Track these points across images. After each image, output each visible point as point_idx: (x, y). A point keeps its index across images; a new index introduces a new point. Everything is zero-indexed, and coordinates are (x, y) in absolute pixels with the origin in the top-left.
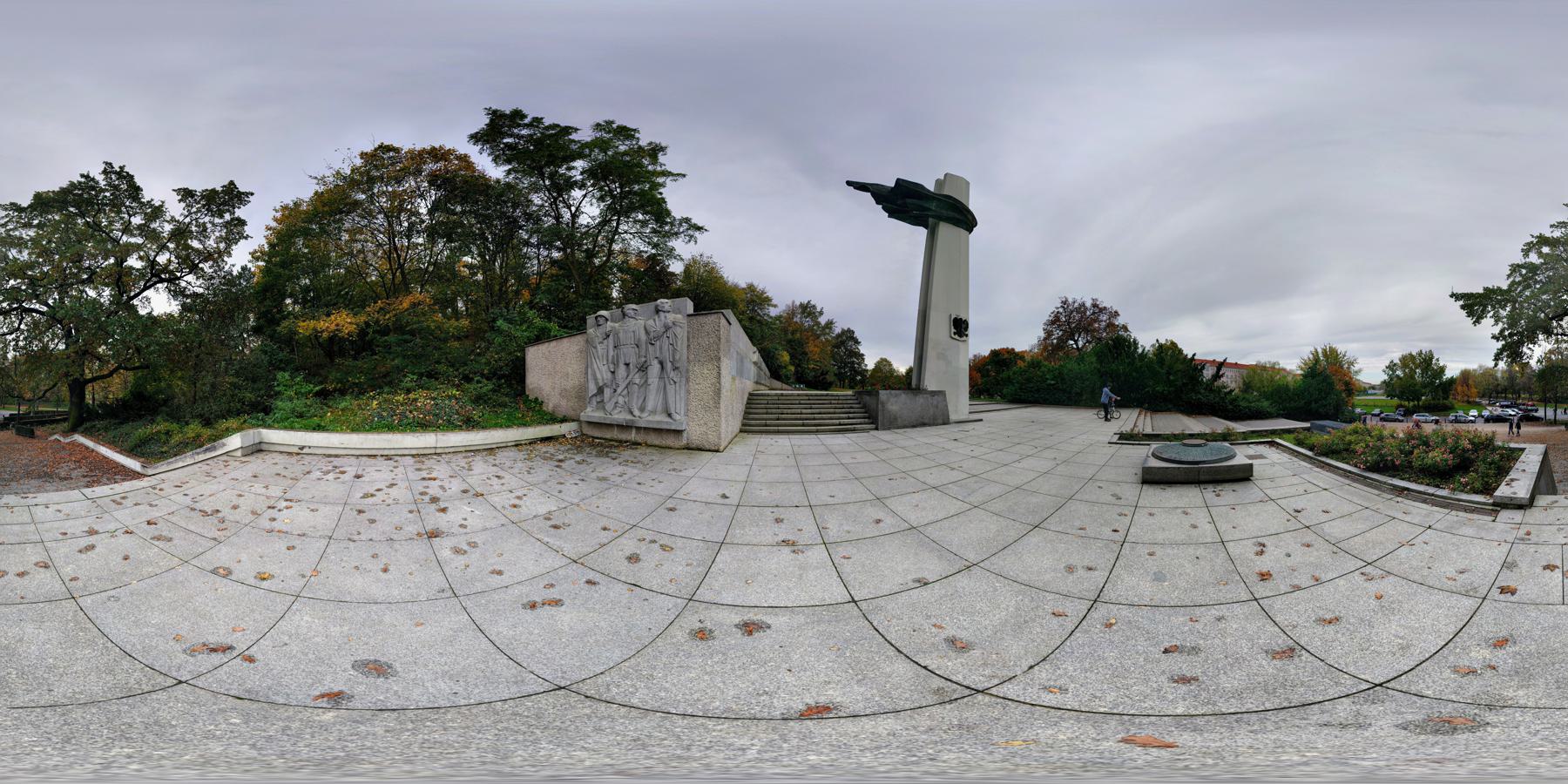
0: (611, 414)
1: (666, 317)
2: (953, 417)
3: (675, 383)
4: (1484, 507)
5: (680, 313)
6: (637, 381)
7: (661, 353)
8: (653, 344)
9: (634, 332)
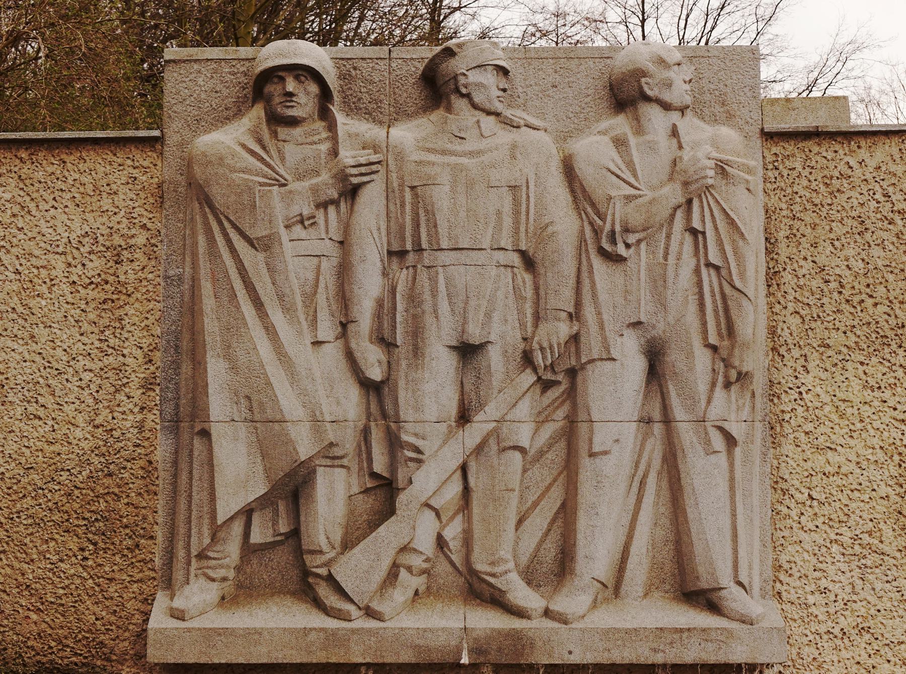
0: (370, 613)
1: (674, 132)
2: (387, 618)
3: (730, 441)
4: (238, 285)
5: (729, 118)
6: (524, 435)
7: (662, 303)
8: (618, 259)
9: (513, 188)
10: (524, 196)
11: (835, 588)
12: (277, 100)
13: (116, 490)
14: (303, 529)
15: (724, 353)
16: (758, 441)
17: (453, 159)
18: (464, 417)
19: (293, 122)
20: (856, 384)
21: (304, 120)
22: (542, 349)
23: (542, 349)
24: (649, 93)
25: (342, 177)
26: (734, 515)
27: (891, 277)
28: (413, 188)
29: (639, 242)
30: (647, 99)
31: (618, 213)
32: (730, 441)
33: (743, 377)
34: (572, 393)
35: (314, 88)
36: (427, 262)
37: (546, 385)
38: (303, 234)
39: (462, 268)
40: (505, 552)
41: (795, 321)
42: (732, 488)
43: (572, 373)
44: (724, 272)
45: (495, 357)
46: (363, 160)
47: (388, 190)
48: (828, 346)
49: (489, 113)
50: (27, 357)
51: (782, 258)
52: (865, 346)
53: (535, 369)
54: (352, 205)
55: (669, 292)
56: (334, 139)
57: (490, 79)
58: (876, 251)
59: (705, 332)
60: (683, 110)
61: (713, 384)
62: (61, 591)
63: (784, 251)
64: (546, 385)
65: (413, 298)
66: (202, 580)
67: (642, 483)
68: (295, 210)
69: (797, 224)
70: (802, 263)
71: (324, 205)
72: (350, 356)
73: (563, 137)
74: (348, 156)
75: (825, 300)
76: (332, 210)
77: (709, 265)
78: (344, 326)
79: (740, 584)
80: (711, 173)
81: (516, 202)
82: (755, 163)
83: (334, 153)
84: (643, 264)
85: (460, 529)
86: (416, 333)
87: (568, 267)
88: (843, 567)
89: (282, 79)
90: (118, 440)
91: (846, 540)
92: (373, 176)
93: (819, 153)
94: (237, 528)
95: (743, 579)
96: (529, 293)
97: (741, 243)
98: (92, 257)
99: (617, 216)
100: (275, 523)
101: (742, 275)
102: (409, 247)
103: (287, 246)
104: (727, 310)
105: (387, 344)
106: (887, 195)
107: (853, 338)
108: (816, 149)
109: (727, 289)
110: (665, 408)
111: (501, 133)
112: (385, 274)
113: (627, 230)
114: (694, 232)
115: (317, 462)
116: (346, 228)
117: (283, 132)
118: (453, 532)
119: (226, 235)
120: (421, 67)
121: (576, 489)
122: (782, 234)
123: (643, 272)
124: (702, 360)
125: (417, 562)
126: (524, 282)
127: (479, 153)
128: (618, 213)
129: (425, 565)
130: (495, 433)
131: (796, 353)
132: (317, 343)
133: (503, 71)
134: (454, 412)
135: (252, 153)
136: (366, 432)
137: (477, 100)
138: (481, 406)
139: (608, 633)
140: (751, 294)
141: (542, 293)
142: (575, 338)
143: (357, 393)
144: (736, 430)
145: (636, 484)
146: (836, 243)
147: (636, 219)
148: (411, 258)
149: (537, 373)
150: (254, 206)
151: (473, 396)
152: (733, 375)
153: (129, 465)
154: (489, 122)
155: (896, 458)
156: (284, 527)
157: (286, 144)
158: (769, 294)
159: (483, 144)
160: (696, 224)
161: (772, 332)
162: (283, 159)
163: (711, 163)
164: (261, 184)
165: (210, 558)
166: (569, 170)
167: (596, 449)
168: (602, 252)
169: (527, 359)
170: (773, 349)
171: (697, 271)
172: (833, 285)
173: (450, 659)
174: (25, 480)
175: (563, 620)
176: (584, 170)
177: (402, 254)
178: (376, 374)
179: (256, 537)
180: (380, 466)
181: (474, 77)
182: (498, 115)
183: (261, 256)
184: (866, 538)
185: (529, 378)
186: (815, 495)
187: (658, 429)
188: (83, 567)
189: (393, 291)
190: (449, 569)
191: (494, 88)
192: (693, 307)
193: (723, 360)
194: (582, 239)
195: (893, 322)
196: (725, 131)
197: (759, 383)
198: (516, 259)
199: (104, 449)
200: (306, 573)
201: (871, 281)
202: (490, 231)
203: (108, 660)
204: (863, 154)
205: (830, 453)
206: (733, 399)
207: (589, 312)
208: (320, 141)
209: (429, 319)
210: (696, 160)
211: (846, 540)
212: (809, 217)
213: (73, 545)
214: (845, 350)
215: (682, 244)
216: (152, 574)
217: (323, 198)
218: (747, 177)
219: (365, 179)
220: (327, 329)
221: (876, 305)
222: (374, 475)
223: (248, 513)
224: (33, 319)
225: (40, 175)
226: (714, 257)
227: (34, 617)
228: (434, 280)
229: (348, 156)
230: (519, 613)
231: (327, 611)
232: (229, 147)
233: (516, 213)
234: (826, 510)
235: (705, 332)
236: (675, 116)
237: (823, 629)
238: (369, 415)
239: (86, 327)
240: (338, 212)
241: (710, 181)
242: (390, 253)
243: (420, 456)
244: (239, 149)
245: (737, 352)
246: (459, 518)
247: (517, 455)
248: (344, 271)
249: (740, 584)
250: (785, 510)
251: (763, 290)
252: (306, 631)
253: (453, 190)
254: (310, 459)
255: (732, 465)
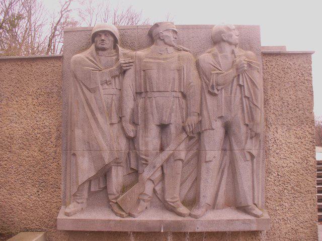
1: (233, 52)
3: (252, 156)
6: (183, 155)
8: (215, 95)
9: (178, 70)
10: (182, 73)
11: (286, 204)
12: (98, 42)
13: (48, 173)
14: (108, 186)
15: (250, 127)
16: (261, 156)
17: (158, 61)
18: (162, 149)
19: (104, 49)
20: (293, 137)
21: (108, 49)
22: (189, 126)
23: (189, 126)
24: (224, 39)
25: (120, 67)
26: (253, 182)
27: (304, 102)
28: (144, 71)
29: (222, 89)
30: (224, 41)
31: (214, 79)
32: (252, 156)
33: (257, 135)
34: (199, 140)
35: (111, 38)
36: (149, 96)
37: (191, 138)
38: (107, 87)
39: (161, 98)
40: (177, 195)
41: (273, 116)
42: (253, 172)
43: (199, 134)
44: (250, 99)
45: (172, 129)
46: (127, 62)
47: (136, 71)
48: (284, 125)
49: (170, 46)
50: (20, 129)
51: (269, 95)
52: (296, 124)
53: (186, 133)
54: (123, 78)
55: (232, 106)
56: (118, 54)
57: (171, 34)
58: (299, 93)
59: (244, 120)
60: (236, 45)
61: (247, 138)
62: (32, 205)
63: (269, 92)
64: (191, 138)
65: (145, 109)
66: (75, 203)
67: (223, 171)
68: (104, 79)
69: (274, 84)
70: (275, 96)
71: (114, 77)
72: (123, 128)
73: (195, 55)
74: (122, 61)
75: (283, 109)
76: (117, 79)
77: (245, 97)
78: (121, 118)
79: (255, 204)
80: (246, 66)
81: (180, 75)
82: (260, 63)
83: (118, 60)
84: (223, 97)
85: (161, 187)
86: (146, 121)
87: (198, 98)
88: (288, 197)
89: (100, 36)
90: (48, 156)
91: (289, 188)
92: (131, 67)
93: (280, 60)
94: (86, 186)
95: (256, 202)
96: (184, 106)
97: (256, 89)
98: (40, 96)
99: (214, 80)
100: (99, 185)
101: (257, 100)
102: (143, 91)
103: (102, 91)
104: (251, 112)
105: (135, 124)
106: (303, 74)
107: (292, 122)
108: (279, 59)
109: (252, 105)
110: (231, 145)
111: (177, 53)
112: (135, 100)
113: (218, 85)
114: (240, 86)
115: (112, 164)
116: (121, 84)
117: (100, 52)
118: (158, 188)
119: (81, 88)
120: (148, 31)
121: (200, 173)
122: (269, 87)
123: (223, 99)
124: (243, 129)
125: (146, 198)
126: (182, 102)
127: (166, 59)
128: (214, 79)
129: (149, 199)
130: (172, 155)
131: (274, 126)
132: (112, 124)
133: (175, 32)
134: (158, 147)
135: (90, 60)
136: (129, 154)
137: (166, 41)
138: (168, 145)
139: (211, 222)
140: (259, 106)
141: (189, 106)
142: (200, 122)
143: (125, 143)
144: (254, 153)
145: (220, 173)
146: (287, 90)
147: (221, 81)
148: (143, 95)
149: (187, 134)
150: (90, 78)
151: (165, 142)
152: (253, 134)
153: (52, 165)
154: (171, 49)
155: (306, 161)
156: (102, 186)
157: (102, 57)
158: (265, 107)
159: (168, 56)
160: (241, 83)
161: (266, 120)
162: (100, 62)
163: (246, 62)
164: (93, 70)
165: (77, 196)
166: (198, 64)
167: (207, 160)
168: (209, 92)
169: (184, 129)
170: (266, 125)
171: (241, 99)
172: (286, 104)
173: (157, 230)
174: (19, 169)
175: (196, 217)
176: (202, 64)
177: (141, 93)
178: (132, 134)
179: (92, 189)
180: (133, 166)
181: (165, 33)
182: (173, 46)
183: (93, 95)
184: (296, 188)
185: (184, 136)
186: (279, 174)
187: (228, 153)
188: (39, 198)
189: (137, 106)
190: (157, 200)
191: (172, 37)
192: (240, 112)
193: (250, 129)
194: (202, 88)
195: (305, 116)
196: (249, 52)
197: (262, 137)
198: (180, 95)
199: (44, 159)
200: (109, 201)
201: (298, 103)
202: (171, 85)
203: (47, 227)
204: (295, 60)
205: (285, 160)
206: (254, 141)
207: (205, 113)
208: (113, 56)
209: (150, 116)
210: (241, 61)
211: (289, 188)
212: (278, 81)
213: (35, 190)
214: (289, 126)
215: (236, 90)
216: (60, 200)
217: (114, 75)
218: (258, 67)
219: (128, 68)
220: (115, 119)
221: (299, 110)
222: (132, 169)
223: (90, 181)
224: (21, 117)
225: (24, 70)
226: (247, 94)
227: (23, 213)
228: (151, 102)
229: (122, 61)
230: (180, 214)
231: (116, 214)
232: (82, 58)
233: (180, 79)
234: (282, 179)
235: (244, 120)
236: (233, 47)
237: (281, 218)
238: (130, 149)
239: (38, 119)
240: (119, 79)
241: (246, 68)
242: (136, 93)
243: (147, 163)
244: (88, 60)
245: (255, 126)
246: (161, 183)
247: (181, 162)
248: (121, 100)
249: (255, 204)
250: (270, 179)
251: (263, 106)
252: (109, 221)
253: (158, 71)
254: (110, 163)
255: (253, 164)
